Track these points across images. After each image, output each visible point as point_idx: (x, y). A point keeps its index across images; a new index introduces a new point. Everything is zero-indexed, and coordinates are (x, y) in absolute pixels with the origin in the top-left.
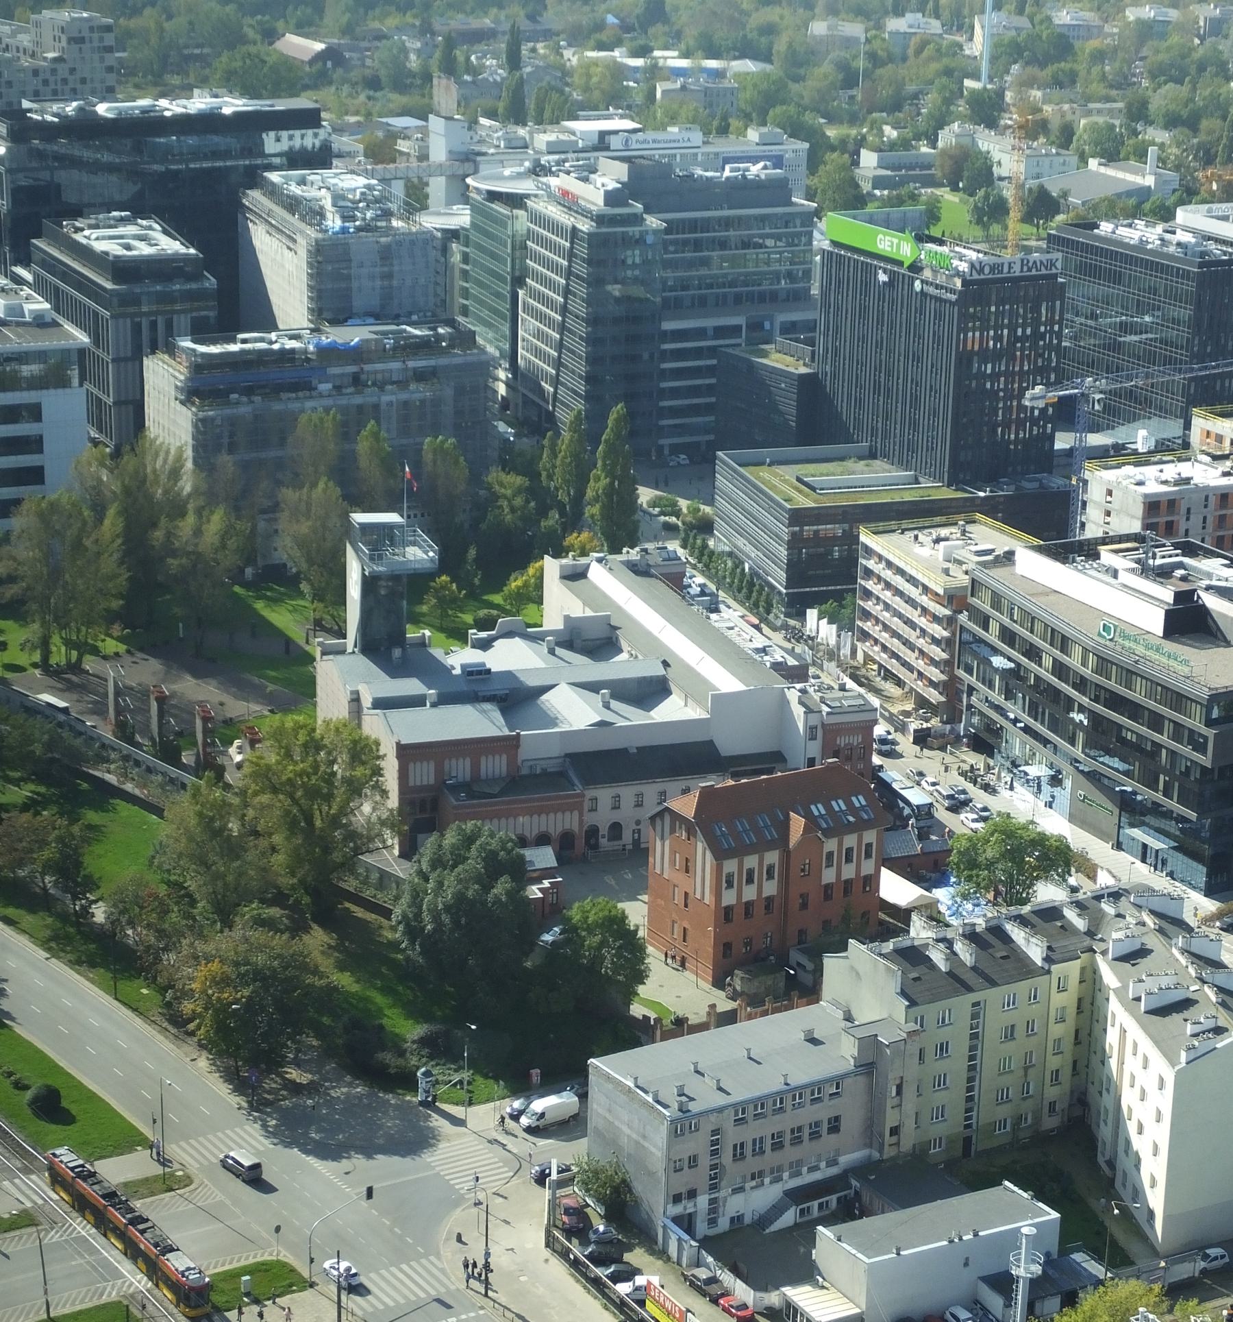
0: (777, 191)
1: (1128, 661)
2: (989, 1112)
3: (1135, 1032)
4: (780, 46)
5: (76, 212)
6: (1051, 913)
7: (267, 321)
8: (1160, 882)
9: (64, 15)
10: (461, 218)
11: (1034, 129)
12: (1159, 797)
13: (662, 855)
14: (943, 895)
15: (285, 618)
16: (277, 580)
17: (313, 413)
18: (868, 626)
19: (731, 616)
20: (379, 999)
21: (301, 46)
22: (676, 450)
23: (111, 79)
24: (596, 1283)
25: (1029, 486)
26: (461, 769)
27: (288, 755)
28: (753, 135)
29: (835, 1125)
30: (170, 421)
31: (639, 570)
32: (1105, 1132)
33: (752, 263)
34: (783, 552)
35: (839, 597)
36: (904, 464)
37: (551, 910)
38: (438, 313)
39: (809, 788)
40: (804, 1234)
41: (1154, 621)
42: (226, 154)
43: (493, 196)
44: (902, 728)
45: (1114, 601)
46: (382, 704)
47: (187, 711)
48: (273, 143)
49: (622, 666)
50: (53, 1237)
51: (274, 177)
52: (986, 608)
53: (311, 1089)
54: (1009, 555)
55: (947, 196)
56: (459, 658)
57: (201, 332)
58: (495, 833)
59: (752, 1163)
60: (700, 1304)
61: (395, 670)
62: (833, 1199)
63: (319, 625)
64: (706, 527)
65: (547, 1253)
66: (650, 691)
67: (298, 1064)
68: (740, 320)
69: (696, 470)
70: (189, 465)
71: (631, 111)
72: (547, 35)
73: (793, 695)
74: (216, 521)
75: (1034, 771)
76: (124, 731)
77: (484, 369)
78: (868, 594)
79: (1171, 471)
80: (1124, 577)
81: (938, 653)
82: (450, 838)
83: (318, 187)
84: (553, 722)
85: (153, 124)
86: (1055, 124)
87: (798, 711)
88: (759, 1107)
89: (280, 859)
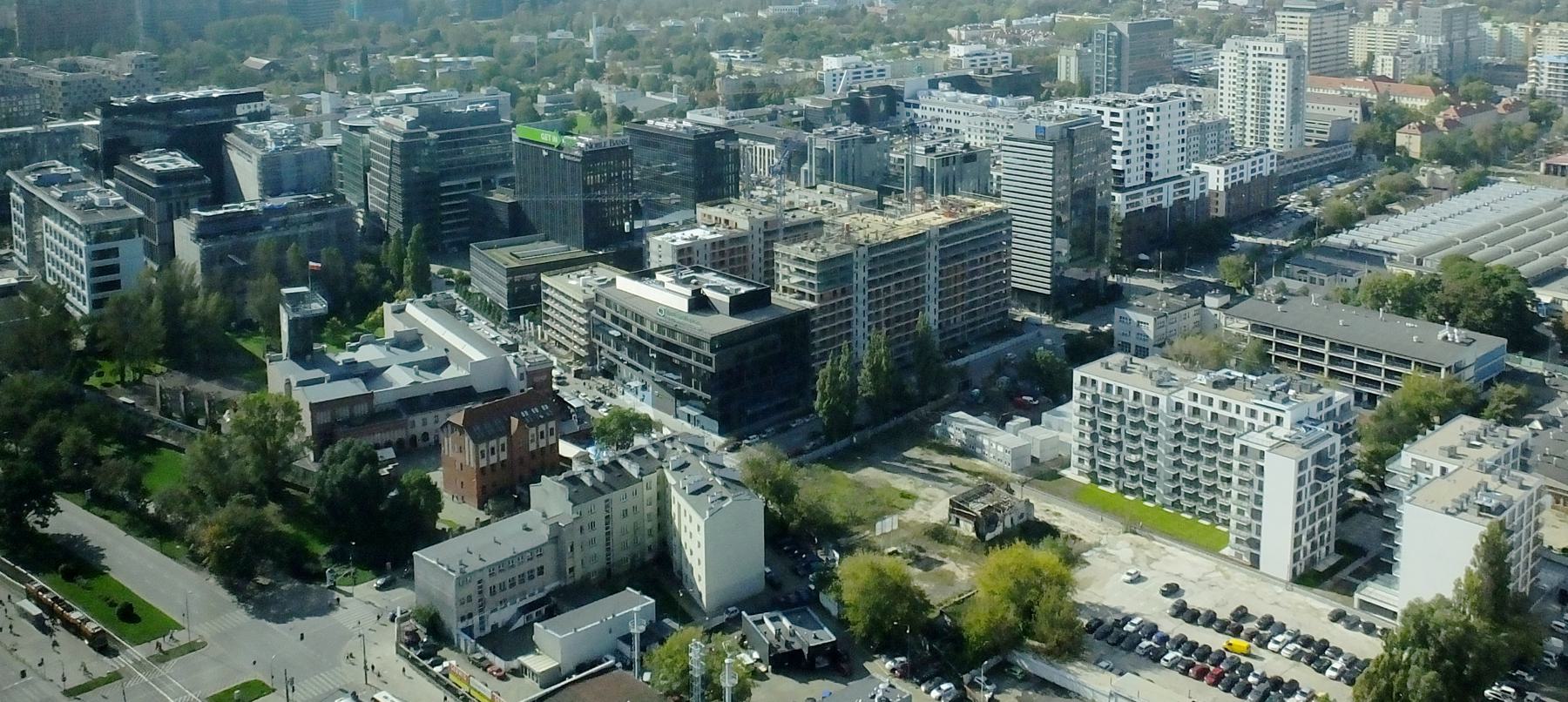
0: (493, 116)
1: (672, 325)
2: (620, 554)
3: (685, 505)
4: (497, 48)
5: (138, 150)
6: (641, 451)
7: (239, 197)
8: (697, 431)
9: (134, 54)
10: (338, 140)
11: (620, 79)
12: (692, 389)
13: (449, 444)
14: (590, 450)
15: (253, 346)
16: (248, 327)
17: (263, 241)
18: (548, 322)
19: (481, 324)
20: (304, 534)
21: (257, 62)
22: (451, 245)
23: (158, 83)
24: (424, 669)
25: (624, 247)
26: (344, 413)
27: (252, 413)
28: (483, 91)
29: (541, 571)
30: (188, 251)
31: (432, 305)
32: (675, 556)
33: (484, 151)
34: (506, 290)
35: (534, 309)
36: (563, 241)
37: (393, 480)
38: (328, 185)
39: (524, 402)
40: (528, 629)
41: (683, 305)
42: (216, 117)
43: (352, 128)
44: (569, 370)
45: (664, 296)
46: (302, 384)
47: (200, 398)
48: (241, 109)
49: (425, 353)
50: (131, 683)
51: (240, 126)
52: (604, 306)
53: (270, 587)
54: (614, 280)
55: (579, 113)
56: (342, 357)
57: (203, 205)
58: (363, 442)
59: (499, 596)
60: (478, 672)
61: (308, 366)
62: (543, 609)
63: (269, 348)
64: (467, 281)
65: (397, 657)
66: (440, 364)
67: (263, 575)
68: (479, 179)
69: (460, 253)
70: (199, 272)
71: (423, 83)
72: (381, 50)
73: (511, 359)
74: (214, 298)
75: (633, 384)
76: (165, 411)
77: (350, 213)
78: (547, 306)
79: (688, 234)
80: (667, 286)
81: (583, 331)
82: (338, 448)
83: (262, 130)
84: (391, 384)
85: (177, 104)
86: (629, 77)
87: (514, 367)
88: (501, 566)
89: (250, 467)
